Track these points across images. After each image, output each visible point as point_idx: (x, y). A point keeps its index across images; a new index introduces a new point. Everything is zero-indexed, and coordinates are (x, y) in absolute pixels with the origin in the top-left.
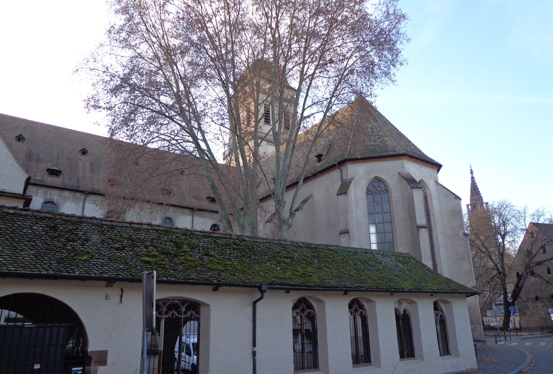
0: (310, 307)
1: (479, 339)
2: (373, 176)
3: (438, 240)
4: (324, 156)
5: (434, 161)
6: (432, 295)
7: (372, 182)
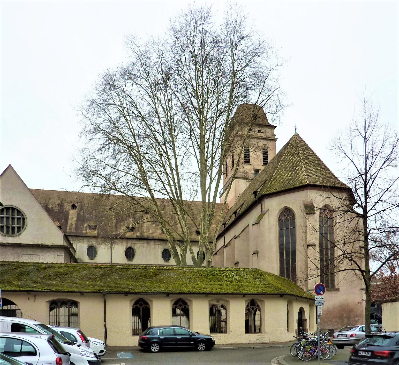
0: (185, 303)
4: (258, 193)
6: (244, 296)
7: (40, 247)
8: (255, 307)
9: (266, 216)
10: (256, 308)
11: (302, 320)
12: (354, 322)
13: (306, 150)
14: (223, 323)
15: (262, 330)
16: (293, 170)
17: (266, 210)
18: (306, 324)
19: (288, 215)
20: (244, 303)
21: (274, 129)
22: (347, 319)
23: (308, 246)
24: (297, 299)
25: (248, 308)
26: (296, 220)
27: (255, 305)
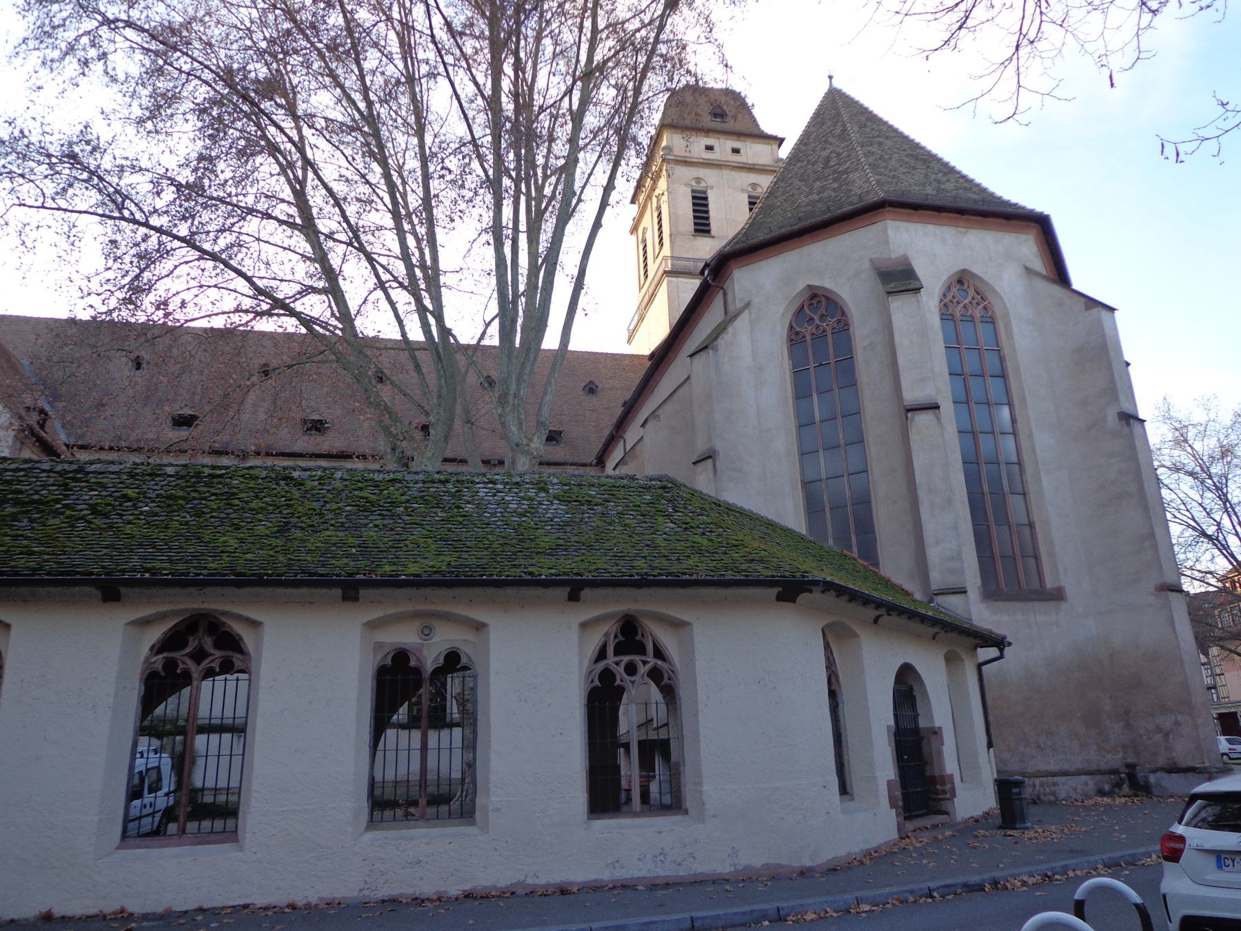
1: (1190, 764)
2: (801, 285)
3: (1033, 449)
5: (1023, 208)
8: (645, 663)
9: (738, 323)
10: (648, 666)
11: (916, 731)
12: (1158, 737)
13: (868, 124)
14: (622, 749)
15: (689, 801)
16: (829, 175)
17: (739, 305)
18: (940, 754)
19: (822, 317)
20: (574, 633)
21: (779, 146)
22: (1121, 724)
23: (909, 410)
24: (876, 621)
25: (601, 665)
26: (851, 329)
27: (641, 650)
